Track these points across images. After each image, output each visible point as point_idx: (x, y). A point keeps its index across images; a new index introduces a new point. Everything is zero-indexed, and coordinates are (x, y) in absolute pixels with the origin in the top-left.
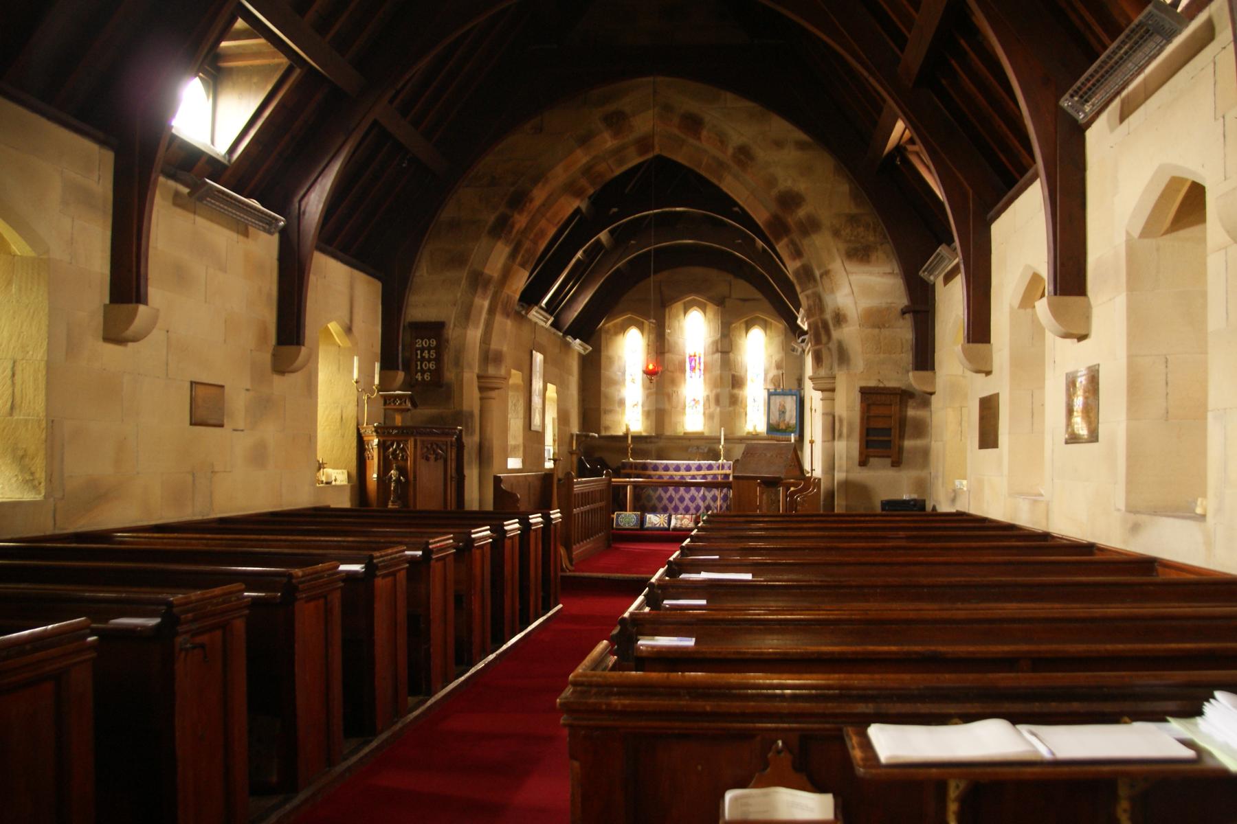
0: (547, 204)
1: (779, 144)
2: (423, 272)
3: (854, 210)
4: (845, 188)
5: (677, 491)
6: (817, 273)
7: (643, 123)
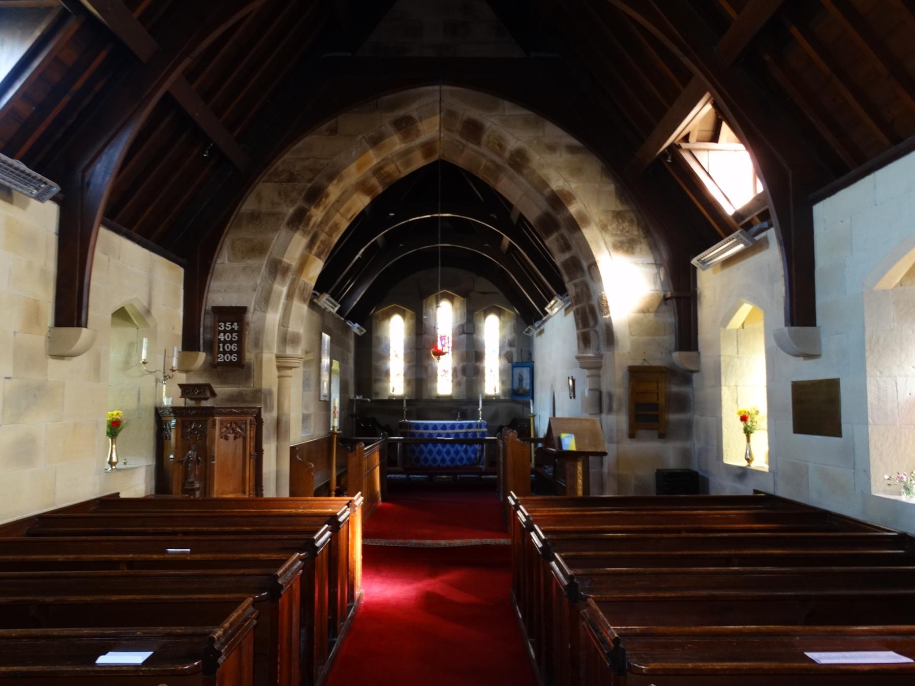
0: (340, 201)
1: (552, 148)
2: (224, 261)
3: (620, 208)
4: (611, 187)
5: (443, 447)
6: (585, 264)
7: (429, 128)
